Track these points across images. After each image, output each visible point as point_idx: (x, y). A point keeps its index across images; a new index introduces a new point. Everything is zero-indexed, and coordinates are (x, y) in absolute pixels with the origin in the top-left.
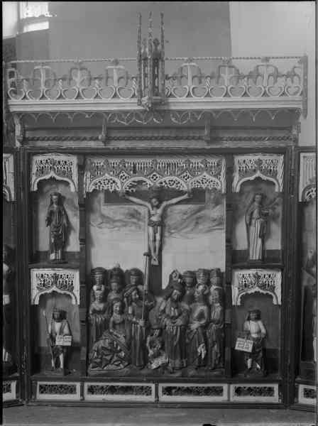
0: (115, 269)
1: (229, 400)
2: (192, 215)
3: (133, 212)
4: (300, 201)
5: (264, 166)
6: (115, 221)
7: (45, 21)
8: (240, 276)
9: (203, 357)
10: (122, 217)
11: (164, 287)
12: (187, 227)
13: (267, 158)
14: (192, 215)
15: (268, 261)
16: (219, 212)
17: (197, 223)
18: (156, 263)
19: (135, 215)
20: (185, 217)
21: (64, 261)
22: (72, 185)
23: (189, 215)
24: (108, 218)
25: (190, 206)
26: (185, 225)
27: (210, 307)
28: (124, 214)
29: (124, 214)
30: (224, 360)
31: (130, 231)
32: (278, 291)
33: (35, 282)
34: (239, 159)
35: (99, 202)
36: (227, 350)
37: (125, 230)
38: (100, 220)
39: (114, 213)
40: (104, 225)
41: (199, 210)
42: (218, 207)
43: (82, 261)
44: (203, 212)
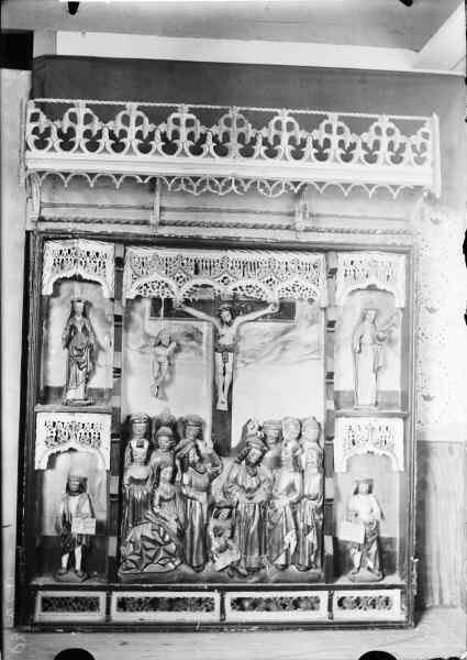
2: (276, 338)
14: (276, 338)
18: (223, 407)
35: (143, 316)
36: (328, 541)
41: (285, 332)
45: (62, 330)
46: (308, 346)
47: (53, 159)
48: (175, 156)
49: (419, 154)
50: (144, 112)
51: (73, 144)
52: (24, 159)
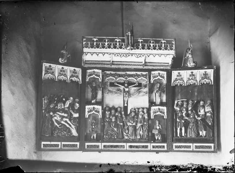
0: (112, 107)
1: (150, 150)
2: (137, 91)
3: (118, 89)
4: (172, 85)
5: (160, 75)
6: (113, 92)
7: (151, 108)
8: (153, 108)
9: (142, 135)
10: (115, 91)
11: (128, 113)
12: (136, 94)
13: (161, 72)
14: (137, 91)
15: (162, 104)
16: (146, 90)
17: (139, 93)
18: (126, 105)
19: (119, 90)
20: (135, 91)
21: (97, 103)
22: (100, 79)
23: (136, 91)
24: (110, 91)
25: (136, 88)
26: (135, 94)
27: (160, 171)
28: (116, 90)
29: (116, 90)
30: (149, 136)
31: (118, 95)
32: (166, 114)
33: (87, 110)
34: (153, 72)
35: (108, 86)
36: (150, 133)
37: (116, 95)
38: (108, 92)
39: (113, 89)
40: (109, 93)
41: (140, 89)
42: (146, 88)
43: (101, 103)
44: (141, 90)
45: (170, 165)
46: (145, 92)
47: (202, 74)
48: (104, 49)
49: (103, 45)
50: (154, 41)
51: (88, 47)
52: (83, 49)
